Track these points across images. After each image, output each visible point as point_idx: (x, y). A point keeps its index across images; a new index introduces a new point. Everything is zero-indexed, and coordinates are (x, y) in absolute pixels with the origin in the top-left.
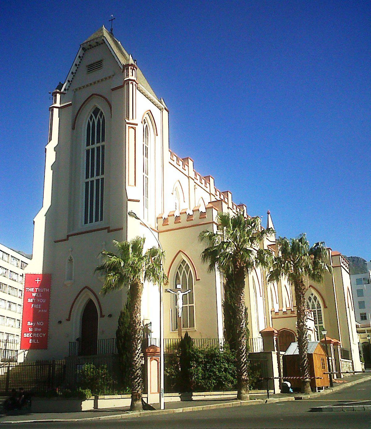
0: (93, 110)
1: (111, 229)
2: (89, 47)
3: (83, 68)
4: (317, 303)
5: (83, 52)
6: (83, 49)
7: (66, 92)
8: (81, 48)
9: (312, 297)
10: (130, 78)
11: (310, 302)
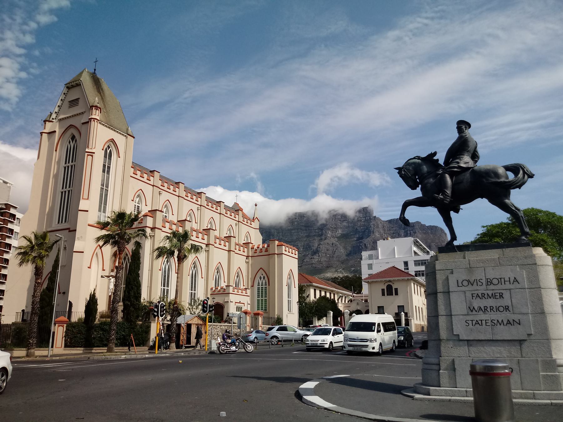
0: (71, 137)
1: (68, 230)
2: (76, 85)
3: (66, 104)
4: (261, 281)
5: (68, 90)
6: (67, 87)
7: (54, 120)
8: (65, 88)
9: (262, 277)
10: (93, 117)
11: (260, 280)
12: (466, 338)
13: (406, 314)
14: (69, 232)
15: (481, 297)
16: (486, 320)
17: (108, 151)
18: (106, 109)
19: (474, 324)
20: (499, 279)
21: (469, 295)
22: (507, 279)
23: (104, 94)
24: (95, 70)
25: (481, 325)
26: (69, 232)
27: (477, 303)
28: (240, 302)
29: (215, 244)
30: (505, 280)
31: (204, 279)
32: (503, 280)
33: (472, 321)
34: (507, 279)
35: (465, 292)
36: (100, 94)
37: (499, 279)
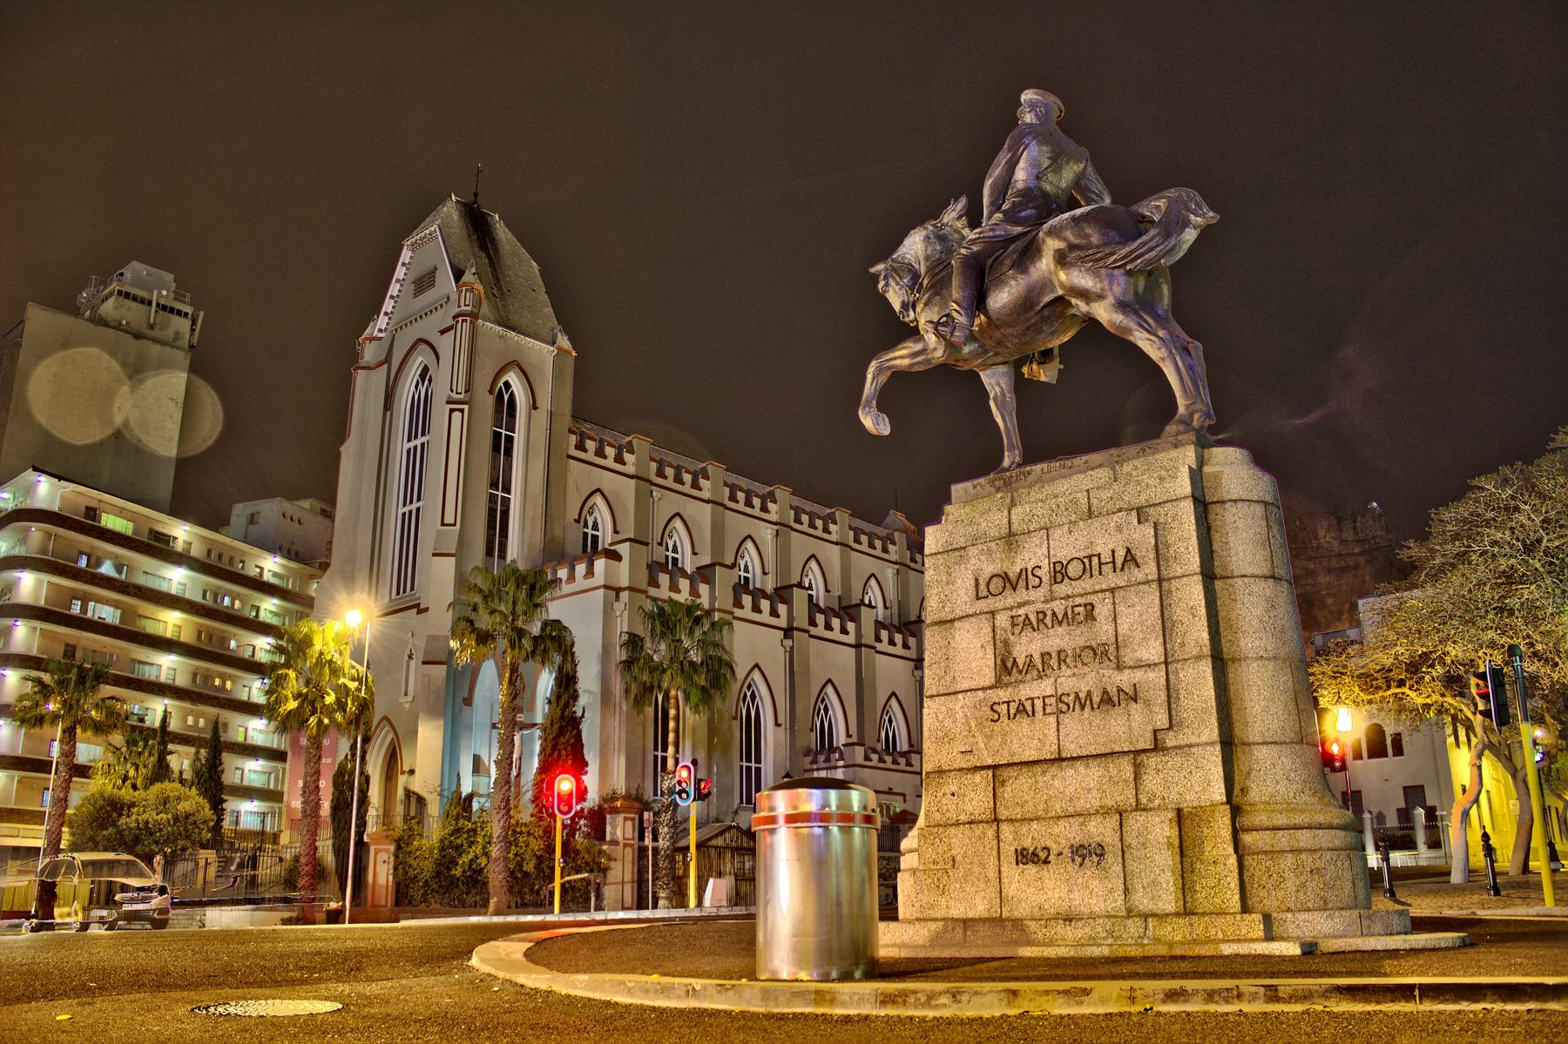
12: (990, 762)
13: (1431, 814)
14: (418, 613)
15: (1035, 623)
16: (1044, 697)
17: (506, 397)
18: (500, 289)
19: (1012, 711)
20: (1086, 560)
21: (1002, 620)
22: (1106, 557)
23: (497, 251)
24: (476, 195)
25: (1030, 713)
26: (418, 613)
27: (1027, 647)
28: (890, 789)
29: (811, 628)
30: (1102, 561)
31: (783, 726)
32: (1095, 560)
33: (1008, 703)
34: (1106, 557)
35: (993, 613)
36: (486, 251)
37: (1086, 560)
